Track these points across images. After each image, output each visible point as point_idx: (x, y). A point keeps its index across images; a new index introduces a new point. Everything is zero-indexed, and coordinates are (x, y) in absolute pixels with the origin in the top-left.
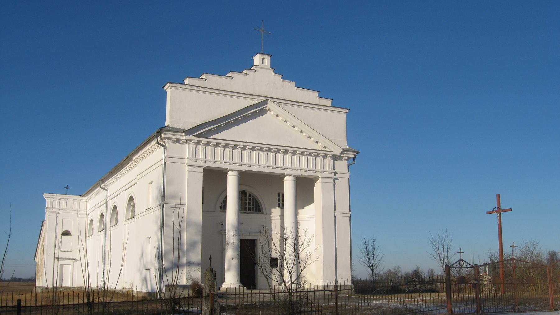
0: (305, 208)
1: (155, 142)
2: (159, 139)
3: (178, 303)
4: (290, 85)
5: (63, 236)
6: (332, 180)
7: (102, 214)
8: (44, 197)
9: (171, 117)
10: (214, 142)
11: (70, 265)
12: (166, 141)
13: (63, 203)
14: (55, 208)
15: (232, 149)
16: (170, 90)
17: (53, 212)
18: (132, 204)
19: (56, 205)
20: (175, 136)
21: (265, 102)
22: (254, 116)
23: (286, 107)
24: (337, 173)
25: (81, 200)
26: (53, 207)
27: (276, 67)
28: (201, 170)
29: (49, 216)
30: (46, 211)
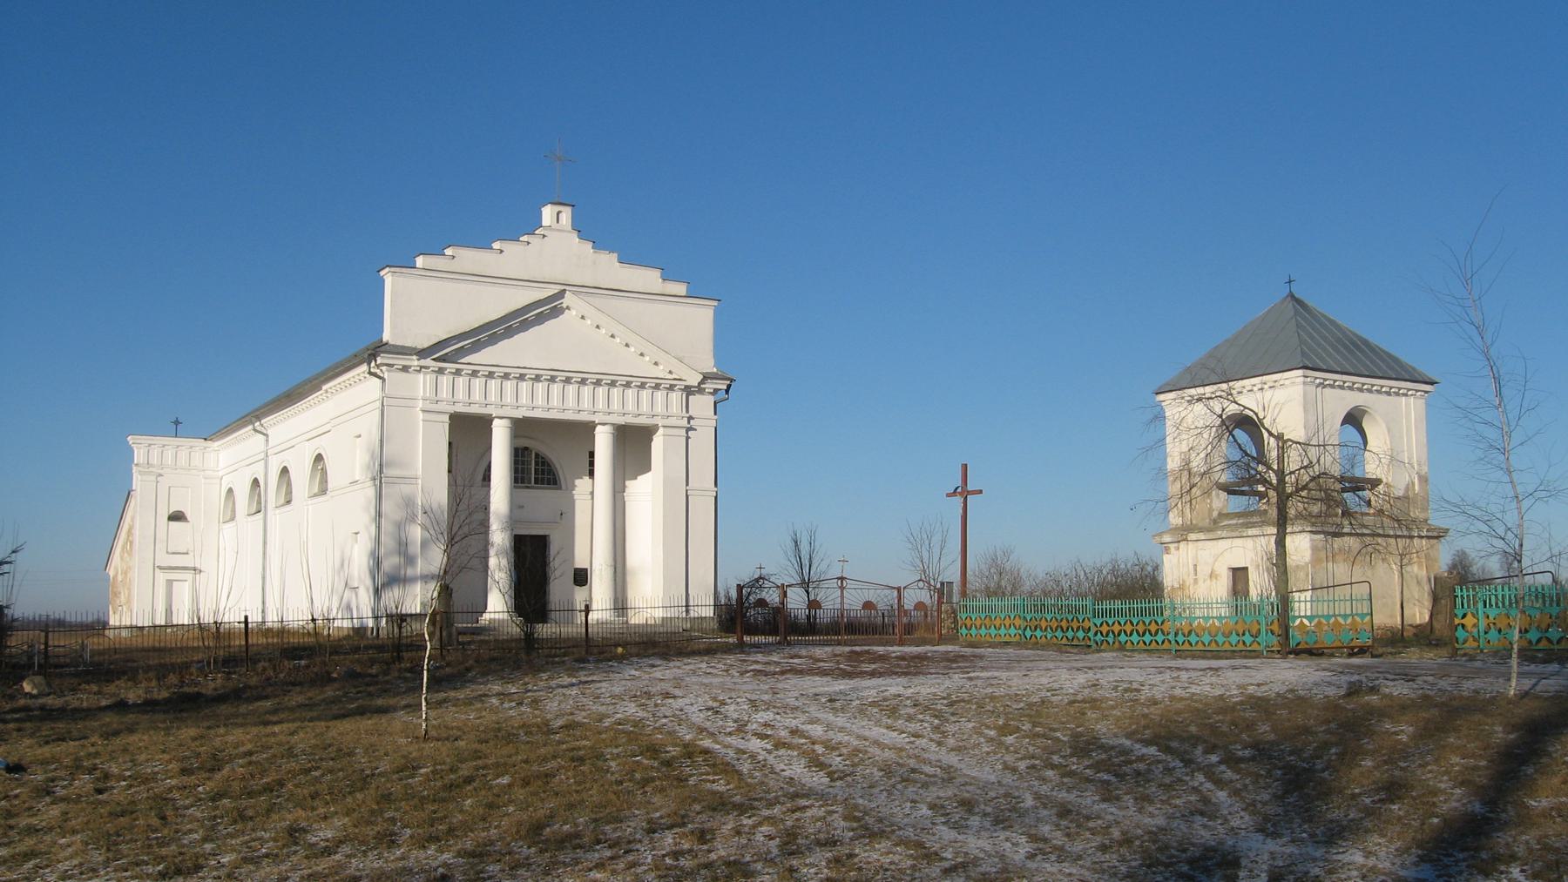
0: (639, 478)
1: (364, 367)
2: (373, 364)
3: (405, 620)
4: (609, 260)
5: (171, 523)
6: (683, 432)
7: (256, 482)
8: (128, 442)
9: (393, 327)
10: (468, 369)
11: (186, 581)
12: (384, 368)
13: (169, 454)
14: (152, 466)
15: (500, 380)
16: (389, 278)
17: (150, 473)
18: (319, 467)
19: (155, 460)
20: (400, 361)
21: (561, 294)
22: (541, 319)
23: (597, 301)
24: (693, 419)
25: (205, 448)
26: (148, 463)
27: (581, 229)
28: (446, 418)
29: (141, 481)
30: (134, 471)
